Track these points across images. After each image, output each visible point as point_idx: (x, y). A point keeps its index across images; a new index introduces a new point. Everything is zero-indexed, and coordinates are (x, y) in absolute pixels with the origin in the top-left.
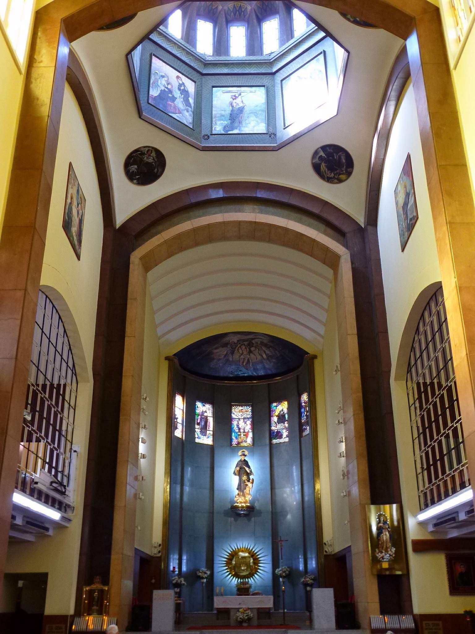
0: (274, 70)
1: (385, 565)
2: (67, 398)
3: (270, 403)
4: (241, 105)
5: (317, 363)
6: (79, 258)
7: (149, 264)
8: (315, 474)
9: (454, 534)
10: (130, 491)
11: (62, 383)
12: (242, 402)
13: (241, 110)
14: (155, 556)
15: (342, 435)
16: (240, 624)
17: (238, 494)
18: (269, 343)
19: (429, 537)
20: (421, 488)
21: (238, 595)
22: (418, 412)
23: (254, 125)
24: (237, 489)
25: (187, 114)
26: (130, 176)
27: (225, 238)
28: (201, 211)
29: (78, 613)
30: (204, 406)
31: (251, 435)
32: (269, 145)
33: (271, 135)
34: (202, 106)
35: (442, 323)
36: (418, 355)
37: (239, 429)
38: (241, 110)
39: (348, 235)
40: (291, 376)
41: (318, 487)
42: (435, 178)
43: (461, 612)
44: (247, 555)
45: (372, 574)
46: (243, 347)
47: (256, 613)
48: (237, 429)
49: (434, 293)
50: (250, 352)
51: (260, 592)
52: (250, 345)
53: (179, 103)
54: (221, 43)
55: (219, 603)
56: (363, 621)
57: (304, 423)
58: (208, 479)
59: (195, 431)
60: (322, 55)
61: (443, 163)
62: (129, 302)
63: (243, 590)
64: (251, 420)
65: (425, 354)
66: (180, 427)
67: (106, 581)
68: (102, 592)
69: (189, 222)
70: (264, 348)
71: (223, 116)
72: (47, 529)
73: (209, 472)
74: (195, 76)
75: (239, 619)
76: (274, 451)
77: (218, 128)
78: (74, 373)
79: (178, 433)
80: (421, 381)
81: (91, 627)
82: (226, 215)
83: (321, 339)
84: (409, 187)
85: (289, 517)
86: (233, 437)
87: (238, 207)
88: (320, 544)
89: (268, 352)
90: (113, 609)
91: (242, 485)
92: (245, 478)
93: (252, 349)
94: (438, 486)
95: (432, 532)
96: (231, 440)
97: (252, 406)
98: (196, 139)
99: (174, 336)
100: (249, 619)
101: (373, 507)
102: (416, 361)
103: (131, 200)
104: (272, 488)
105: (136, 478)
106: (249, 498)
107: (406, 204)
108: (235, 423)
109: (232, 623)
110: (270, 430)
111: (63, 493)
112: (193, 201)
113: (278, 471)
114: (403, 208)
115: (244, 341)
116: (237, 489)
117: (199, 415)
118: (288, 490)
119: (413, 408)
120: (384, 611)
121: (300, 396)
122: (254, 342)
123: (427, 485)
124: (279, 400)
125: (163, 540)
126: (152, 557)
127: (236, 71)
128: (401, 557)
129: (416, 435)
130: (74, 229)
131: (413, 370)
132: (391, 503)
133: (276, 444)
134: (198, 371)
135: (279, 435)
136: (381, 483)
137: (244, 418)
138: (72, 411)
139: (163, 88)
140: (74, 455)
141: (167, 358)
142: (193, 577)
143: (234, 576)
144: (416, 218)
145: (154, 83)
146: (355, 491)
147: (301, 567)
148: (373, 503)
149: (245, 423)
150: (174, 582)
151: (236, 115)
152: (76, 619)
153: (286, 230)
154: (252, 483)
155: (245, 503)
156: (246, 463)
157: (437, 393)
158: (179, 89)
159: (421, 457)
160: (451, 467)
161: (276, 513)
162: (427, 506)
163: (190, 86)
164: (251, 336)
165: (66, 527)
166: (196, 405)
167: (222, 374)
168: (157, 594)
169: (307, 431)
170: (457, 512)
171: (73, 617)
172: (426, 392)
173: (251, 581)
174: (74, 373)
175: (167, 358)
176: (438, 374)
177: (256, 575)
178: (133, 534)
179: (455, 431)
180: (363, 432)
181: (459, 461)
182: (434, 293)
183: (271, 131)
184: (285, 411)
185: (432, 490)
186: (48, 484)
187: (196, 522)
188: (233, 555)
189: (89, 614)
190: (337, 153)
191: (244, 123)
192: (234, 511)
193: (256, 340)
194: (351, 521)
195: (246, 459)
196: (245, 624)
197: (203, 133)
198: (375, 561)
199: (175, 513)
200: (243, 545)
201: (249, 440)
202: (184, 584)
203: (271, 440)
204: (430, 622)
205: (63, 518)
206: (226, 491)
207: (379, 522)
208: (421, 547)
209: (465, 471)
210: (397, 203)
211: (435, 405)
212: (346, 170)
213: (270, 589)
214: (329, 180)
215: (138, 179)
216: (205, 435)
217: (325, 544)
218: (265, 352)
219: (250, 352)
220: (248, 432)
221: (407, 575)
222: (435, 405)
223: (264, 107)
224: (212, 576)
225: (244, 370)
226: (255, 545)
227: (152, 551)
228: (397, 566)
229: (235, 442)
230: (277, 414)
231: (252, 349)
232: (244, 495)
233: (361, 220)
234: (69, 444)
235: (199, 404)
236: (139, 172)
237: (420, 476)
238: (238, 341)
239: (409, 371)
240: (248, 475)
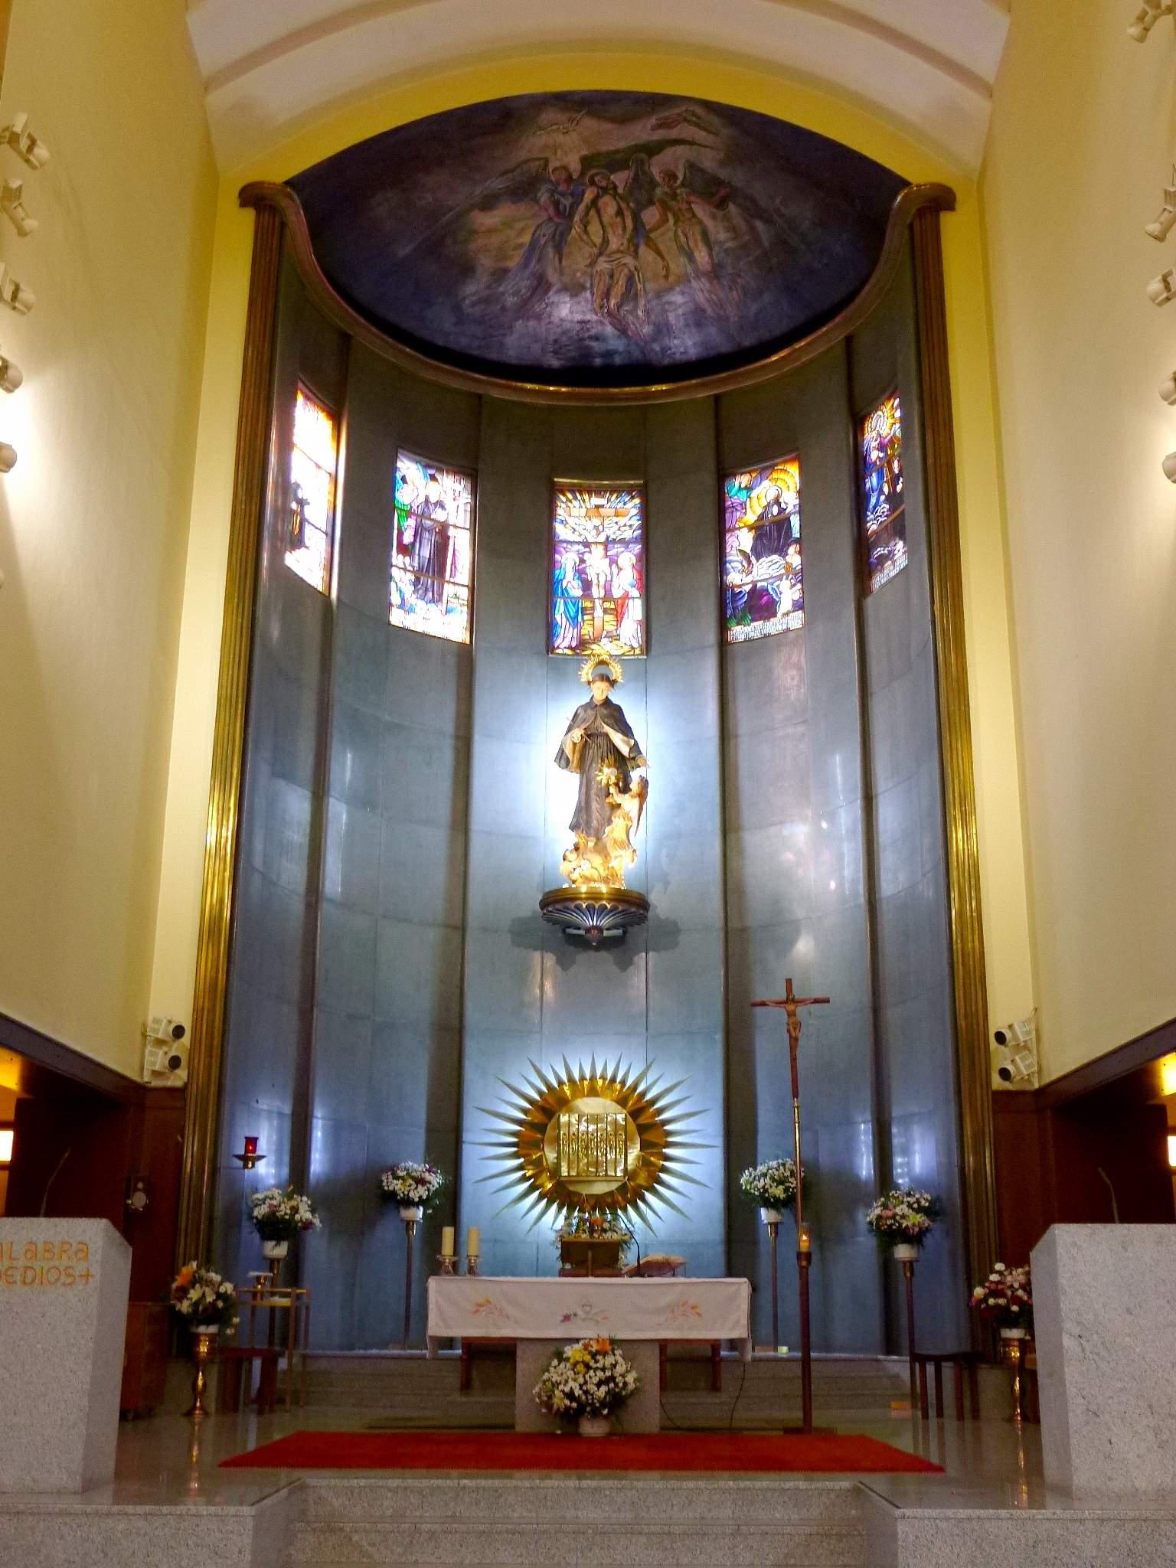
3: (723, 475)
5: (955, 231)
14: (157, 1083)
17: (577, 848)
18: (723, 174)
21: (563, 1273)
24: (574, 827)
30: (433, 478)
31: (635, 610)
37: (587, 586)
47: (653, 1364)
48: (577, 583)
51: (675, 1258)
52: (642, 191)
59: (391, 578)
64: (637, 548)
75: (560, 1401)
76: (739, 671)
79: (310, 562)
85: (804, 947)
86: (559, 616)
88: (968, 1037)
91: (595, 805)
92: (607, 774)
96: (550, 628)
97: (644, 493)
108: (567, 560)
116: (574, 827)
117: (409, 514)
118: (799, 832)
121: (858, 422)
124: (761, 458)
126: (141, 1089)
133: (748, 640)
135: (761, 604)
137: (607, 544)
141: (253, 197)
143: (550, 1197)
147: (865, 1166)
149: (613, 561)
150: (260, 1211)
154: (642, 796)
155: (606, 880)
156: (615, 716)
161: (742, 931)
164: (642, 132)
166: (395, 469)
175: (253, 197)
177: (648, 1196)
184: (791, 500)
188: (547, 1111)
193: (668, 155)
202: (308, 1225)
203: (723, 628)
206: (525, 840)
216: (437, 599)
217: (1000, 1038)
218: (705, 235)
219: (640, 233)
220: (626, 596)
224: (447, 1206)
226: (648, 1068)
229: (565, 639)
230: (751, 518)
231: (651, 216)
232: (601, 849)
235: (408, 467)
238: (587, 162)
240: (623, 763)
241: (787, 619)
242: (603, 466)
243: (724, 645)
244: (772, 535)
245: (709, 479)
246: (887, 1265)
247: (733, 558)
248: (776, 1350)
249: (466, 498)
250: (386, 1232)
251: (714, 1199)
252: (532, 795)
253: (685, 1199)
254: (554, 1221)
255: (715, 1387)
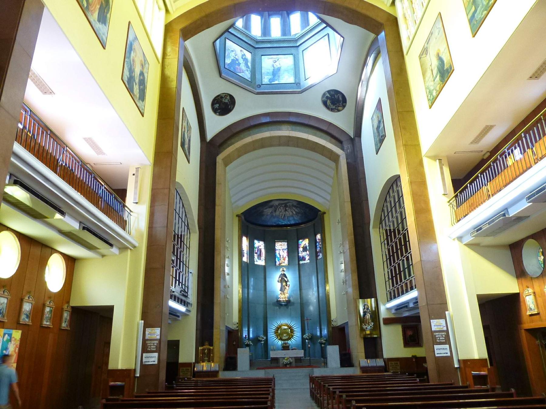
0: (298, 45)
1: (368, 332)
2: (185, 243)
4: (279, 66)
5: (326, 217)
6: (189, 163)
7: (227, 162)
8: (326, 281)
9: (406, 314)
10: (222, 294)
11: (183, 234)
12: (281, 239)
13: (279, 69)
15: (342, 259)
16: (285, 366)
19: (393, 316)
20: (388, 289)
22: (386, 247)
23: (287, 78)
25: (247, 73)
26: (215, 111)
27: (271, 146)
28: (257, 130)
29: (197, 361)
31: (287, 259)
32: (297, 89)
33: (297, 84)
34: (255, 68)
35: (400, 197)
36: (386, 214)
38: (279, 69)
39: (344, 143)
40: (309, 224)
41: (327, 288)
42: (396, 120)
43: (410, 356)
44: (286, 327)
45: (360, 336)
46: (282, 208)
47: (294, 359)
49: (395, 181)
50: (286, 210)
52: (286, 206)
53: (243, 66)
54: (266, 30)
55: (272, 354)
56: (355, 362)
57: (319, 253)
58: (263, 285)
60: (327, 36)
61: (400, 110)
62: (217, 185)
63: (285, 348)
65: (390, 214)
66: (245, 255)
67: (211, 344)
68: (209, 350)
69: (250, 137)
70: (294, 208)
71: (268, 73)
72: (178, 316)
73: (263, 281)
74: (251, 49)
77: (266, 80)
78: (188, 228)
79: (245, 259)
80: (388, 228)
81: (205, 369)
82: (272, 132)
83: (327, 202)
84: (380, 118)
85: (311, 308)
86: (277, 260)
87: (278, 127)
88: (329, 321)
89: (296, 210)
90: (216, 359)
92: (284, 284)
93: (287, 208)
94: (398, 289)
95: (394, 313)
96: (276, 262)
97: (287, 242)
98: (253, 88)
99: (240, 203)
100: (291, 363)
101: (360, 300)
102: (385, 217)
103: (216, 124)
104: (300, 289)
105: (225, 287)
106: (287, 295)
107: (378, 127)
108: (277, 252)
109: (281, 365)
110: (298, 256)
111: (186, 297)
112: (252, 124)
113: (304, 280)
114: (377, 129)
115: (282, 204)
119: (383, 244)
120: (367, 357)
122: (288, 204)
123: (391, 288)
124: (303, 238)
125: (239, 321)
127: (275, 45)
128: (377, 328)
129: (385, 260)
130: (186, 146)
131: (383, 222)
132: (371, 298)
134: (257, 223)
136: (365, 286)
138: (188, 250)
139: (233, 58)
140: (190, 275)
141: (237, 216)
142: (256, 340)
144: (385, 136)
145: (228, 55)
146: (350, 290)
147: (318, 334)
148: (361, 297)
151: (276, 72)
152: (196, 365)
153: (308, 141)
157: (397, 236)
158: (242, 58)
159: (388, 272)
160: (405, 278)
161: (303, 304)
162: (391, 299)
163: (249, 56)
165: (188, 315)
167: (269, 224)
168: (239, 350)
169: (321, 256)
170: (408, 303)
171: (194, 363)
172: (391, 235)
173: (289, 342)
174: (188, 228)
175: (237, 216)
176: (398, 226)
178: (225, 318)
179: (408, 259)
180: (355, 258)
181: (410, 275)
182: (395, 181)
183: (297, 81)
184: (307, 245)
185: (394, 291)
186: (179, 292)
187: (257, 309)
188: (279, 328)
189: (203, 362)
190: (337, 95)
191: (281, 77)
192: (278, 303)
194: (348, 308)
195: (285, 273)
196: (288, 366)
197: (257, 84)
198: (362, 330)
199: (246, 305)
200: (284, 322)
201: (286, 262)
204: (393, 362)
205: (187, 310)
206: (274, 292)
207: (364, 309)
208: (388, 321)
209: (413, 281)
210: (373, 126)
211: (396, 243)
212: (342, 104)
213: (301, 346)
214: (332, 110)
215: (219, 113)
219: (286, 210)
221: (380, 337)
222: (396, 243)
223: (293, 67)
224: (266, 340)
225: (283, 221)
227: (234, 327)
228: (374, 333)
229: (278, 263)
230: (302, 246)
231: (287, 208)
232: (284, 294)
233: (352, 134)
234: (187, 269)
235: (256, 241)
236: (220, 108)
237: (387, 283)
239: (381, 223)
240: (286, 282)
241: (307, 261)
242: (281, 239)
243: (299, 264)
244: (305, 249)
245: (296, 240)
246: (322, 347)
247: (300, 252)
248: (509, 391)
249: (263, 245)
250: (259, 345)
251: (300, 339)
252: (274, 284)
253: (296, 338)
254: (280, 343)
255: (301, 362)
